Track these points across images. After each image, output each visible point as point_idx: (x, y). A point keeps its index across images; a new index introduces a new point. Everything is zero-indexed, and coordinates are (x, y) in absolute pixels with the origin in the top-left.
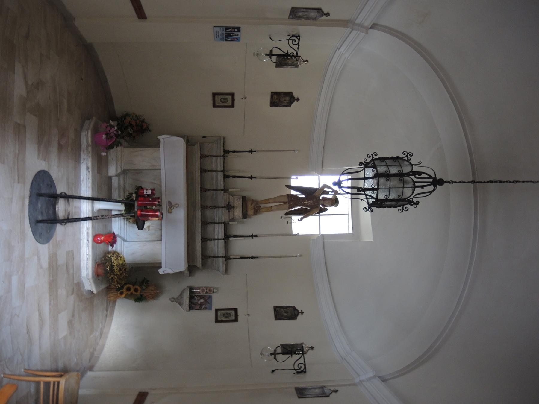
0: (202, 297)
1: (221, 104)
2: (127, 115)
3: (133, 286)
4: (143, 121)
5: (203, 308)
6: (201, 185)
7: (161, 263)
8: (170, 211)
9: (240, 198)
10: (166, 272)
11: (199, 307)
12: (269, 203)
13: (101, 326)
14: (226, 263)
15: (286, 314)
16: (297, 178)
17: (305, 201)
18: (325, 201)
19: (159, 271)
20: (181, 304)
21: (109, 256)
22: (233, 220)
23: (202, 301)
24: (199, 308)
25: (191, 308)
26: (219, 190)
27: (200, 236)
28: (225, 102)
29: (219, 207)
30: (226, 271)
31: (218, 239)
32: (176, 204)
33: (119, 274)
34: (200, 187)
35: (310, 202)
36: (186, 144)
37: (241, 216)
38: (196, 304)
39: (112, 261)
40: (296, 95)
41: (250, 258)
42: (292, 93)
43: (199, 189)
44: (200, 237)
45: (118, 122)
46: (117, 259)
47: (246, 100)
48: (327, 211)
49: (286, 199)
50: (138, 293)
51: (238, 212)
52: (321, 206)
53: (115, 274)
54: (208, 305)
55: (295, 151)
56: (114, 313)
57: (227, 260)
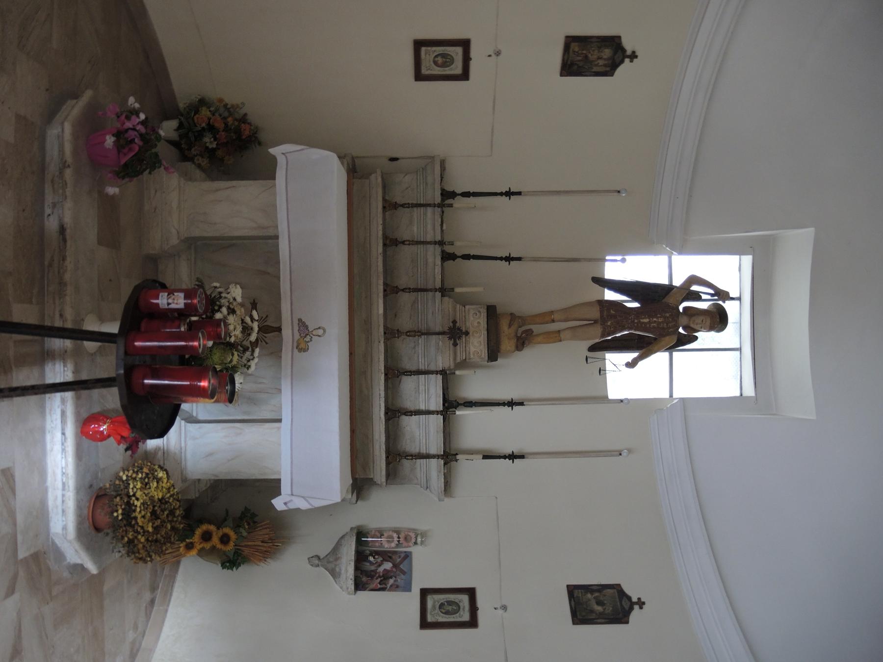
0: (387, 556)
1: (437, 71)
2: (203, 102)
3: (218, 529)
4: (244, 119)
5: (388, 586)
6: (385, 278)
7: (280, 480)
8: (302, 346)
9: (481, 310)
10: (292, 506)
11: (380, 583)
12: (553, 321)
13: (131, 636)
14: (446, 471)
15: (599, 608)
16: (623, 260)
17: (643, 317)
18: (693, 318)
19: (274, 501)
20: (335, 574)
21: (124, 478)
22: (464, 364)
23: (388, 566)
24: (379, 586)
25: (359, 586)
26: (431, 290)
27: (383, 405)
28: (444, 65)
29: (429, 333)
30: (448, 488)
31: (428, 412)
32: (319, 328)
33: (150, 529)
34: (381, 282)
35: (655, 319)
36: (347, 173)
37: (483, 354)
38: (373, 573)
39: (131, 494)
40: (628, 45)
41: (505, 457)
42: (619, 37)
43: (381, 288)
44: (383, 409)
45: (180, 119)
46: (146, 485)
47: (500, 57)
48: (696, 342)
49: (595, 313)
50: (230, 547)
51: (477, 345)
52: (681, 330)
53: (139, 529)
54: (403, 576)
55: (619, 192)
56: (171, 595)
57: (448, 463)
